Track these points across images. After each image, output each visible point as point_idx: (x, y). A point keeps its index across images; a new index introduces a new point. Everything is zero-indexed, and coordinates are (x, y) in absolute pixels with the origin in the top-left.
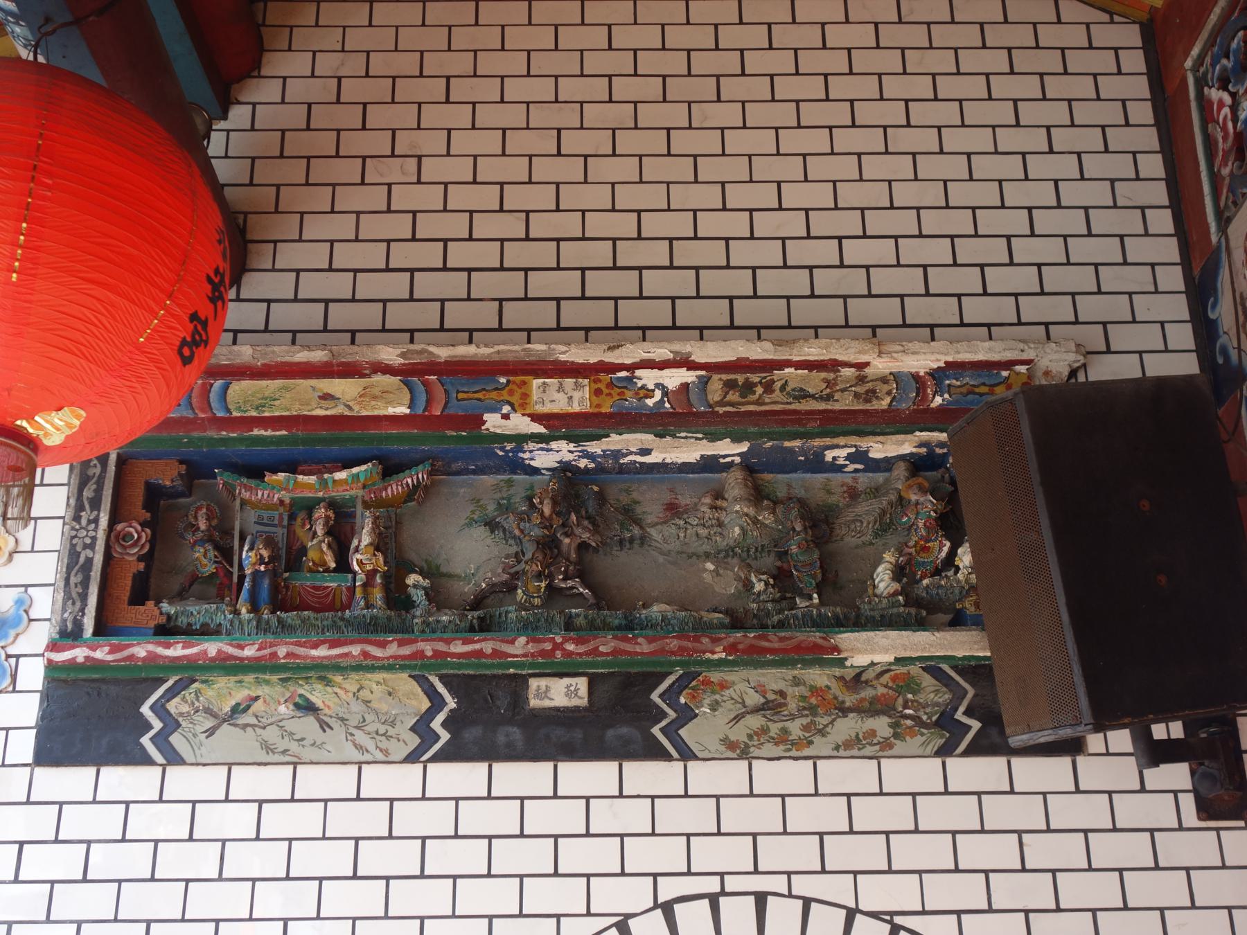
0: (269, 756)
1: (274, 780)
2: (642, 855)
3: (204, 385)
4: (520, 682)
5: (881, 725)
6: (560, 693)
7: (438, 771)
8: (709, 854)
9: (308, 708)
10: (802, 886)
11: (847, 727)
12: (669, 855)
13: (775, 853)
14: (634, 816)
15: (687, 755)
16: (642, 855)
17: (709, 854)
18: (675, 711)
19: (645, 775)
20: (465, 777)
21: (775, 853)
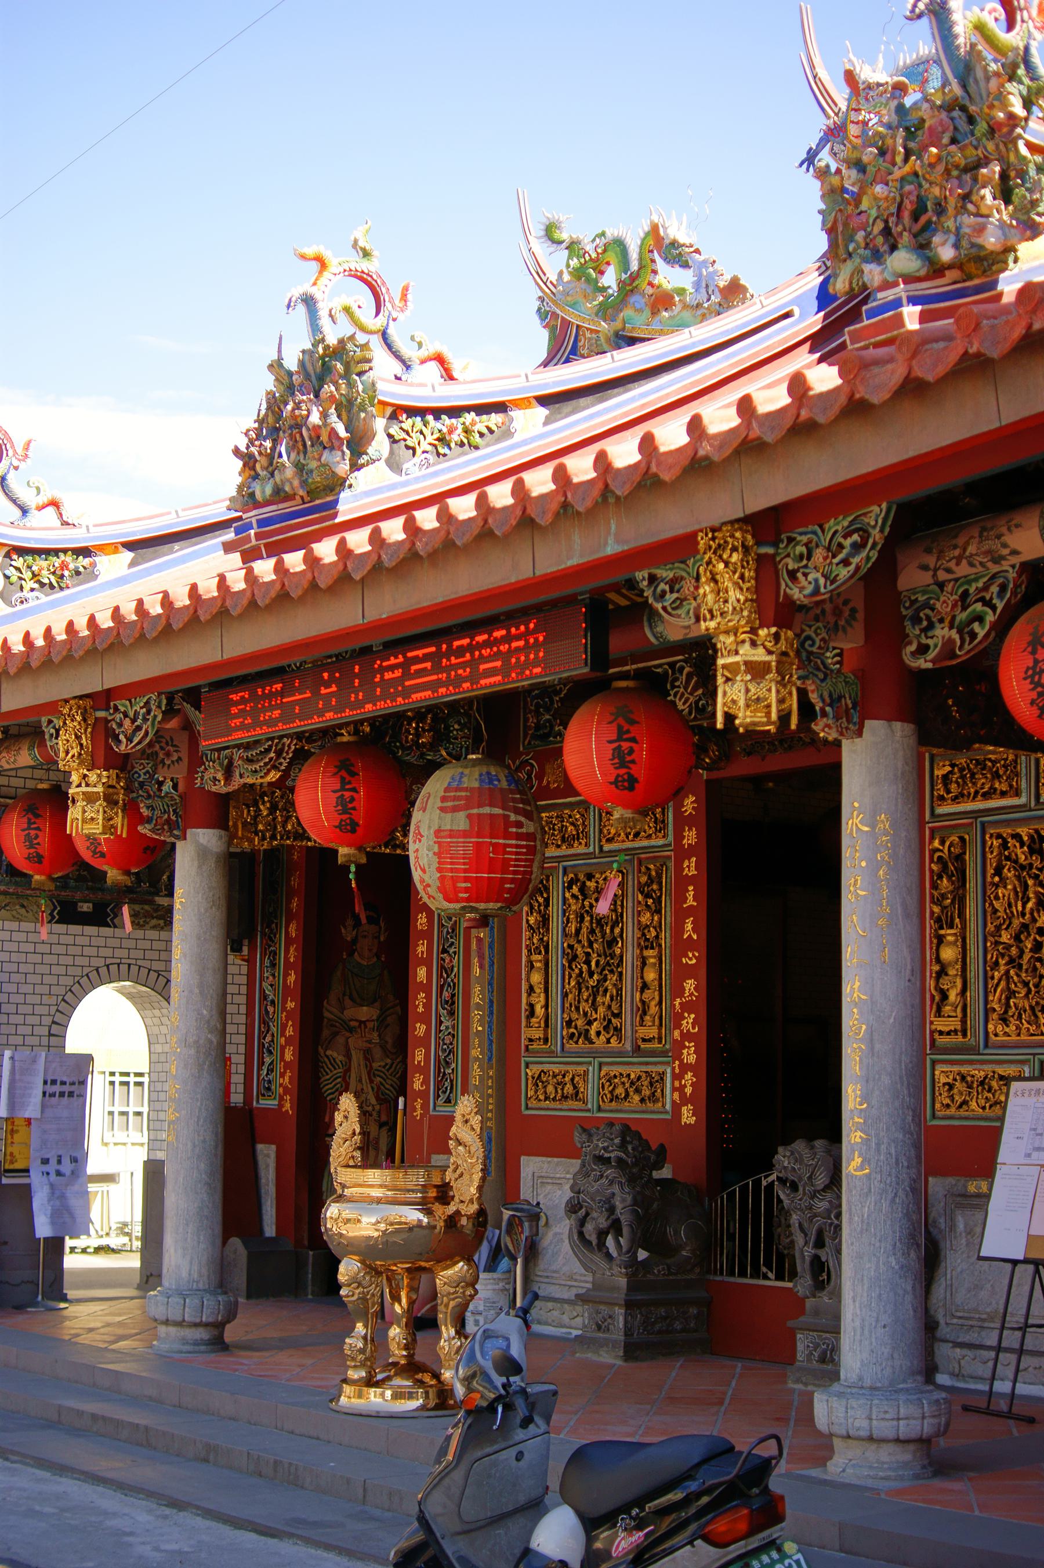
0: (15, 919)
1: (15, 925)
2: (104, 952)
3: (900, 299)
4: (75, 904)
5: (162, 922)
6: (86, 907)
7: (55, 926)
8: (119, 953)
9: (23, 906)
10: (139, 963)
11: (154, 922)
12: (108, 952)
13: (134, 954)
14: (101, 942)
15: (115, 927)
16: (104, 952)
17: (119, 953)
18: (370, 1003)
19: (105, 931)
20: (61, 928)
21: (134, 954)
